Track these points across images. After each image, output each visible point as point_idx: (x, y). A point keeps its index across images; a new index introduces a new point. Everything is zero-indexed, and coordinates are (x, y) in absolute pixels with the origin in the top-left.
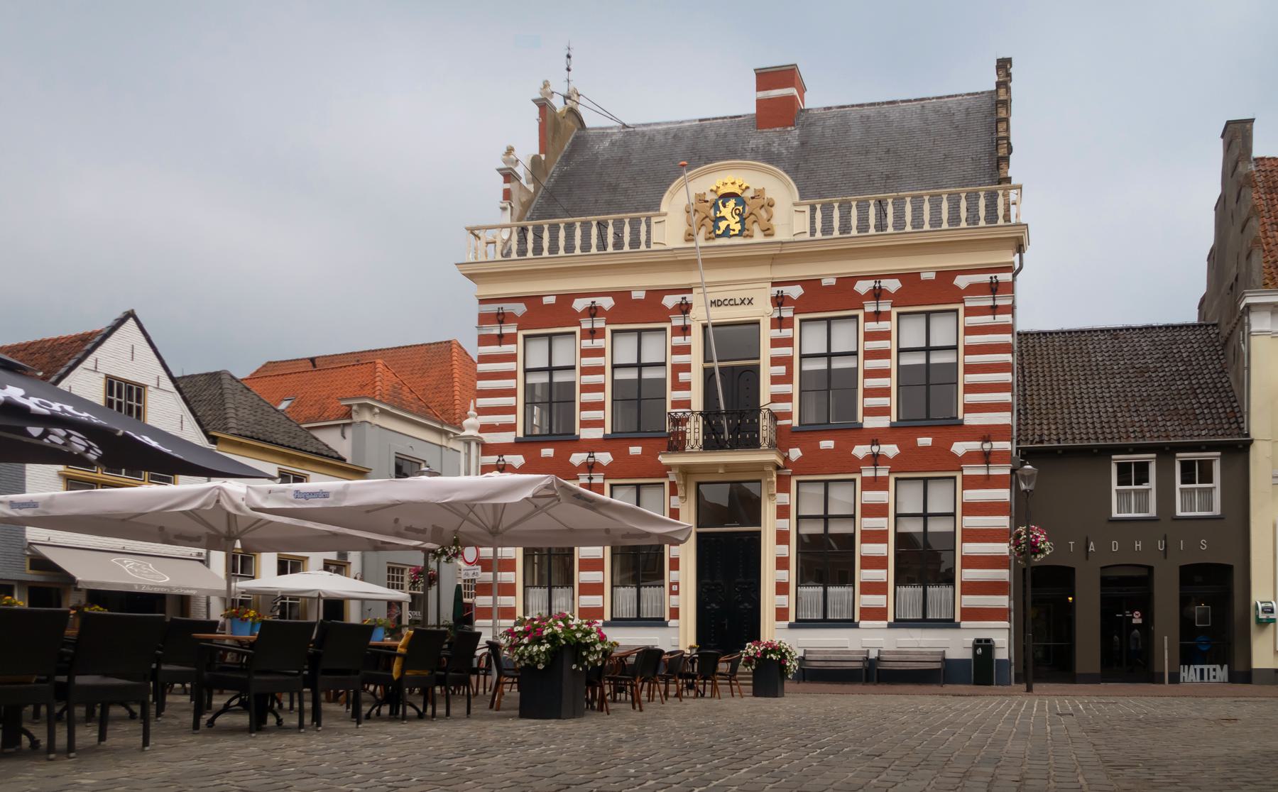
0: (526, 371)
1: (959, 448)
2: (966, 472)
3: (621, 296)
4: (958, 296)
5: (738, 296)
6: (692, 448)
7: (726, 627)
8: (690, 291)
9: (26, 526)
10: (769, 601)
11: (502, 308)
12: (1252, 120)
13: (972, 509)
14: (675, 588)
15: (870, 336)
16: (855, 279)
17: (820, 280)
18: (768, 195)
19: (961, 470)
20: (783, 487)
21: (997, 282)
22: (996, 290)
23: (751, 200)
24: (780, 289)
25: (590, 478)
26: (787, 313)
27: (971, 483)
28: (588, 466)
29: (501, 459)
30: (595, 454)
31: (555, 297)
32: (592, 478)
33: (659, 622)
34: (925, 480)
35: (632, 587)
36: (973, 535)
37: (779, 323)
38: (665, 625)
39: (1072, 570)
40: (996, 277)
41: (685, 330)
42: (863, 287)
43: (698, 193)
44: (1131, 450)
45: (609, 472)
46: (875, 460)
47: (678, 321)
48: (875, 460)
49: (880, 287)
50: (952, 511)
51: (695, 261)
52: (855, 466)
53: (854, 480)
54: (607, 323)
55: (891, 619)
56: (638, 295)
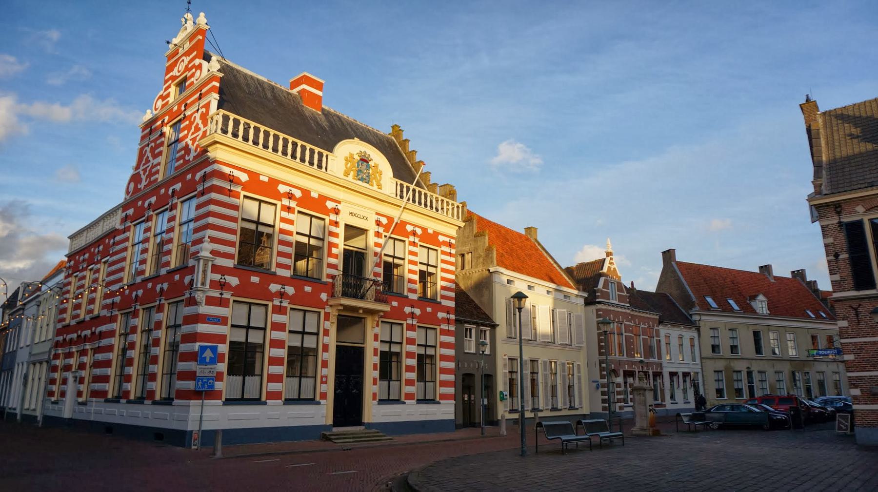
1: (441, 315)
3: (306, 192)
4: (440, 244)
5: (362, 214)
8: (339, 202)
12: (416, 152)
13: (444, 345)
16: (327, 198)
18: (380, 168)
19: (440, 326)
23: (373, 168)
24: (379, 217)
28: (221, 285)
29: (223, 277)
30: (285, 287)
32: (280, 302)
33: (311, 401)
35: (240, 376)
36: (444, 358)
43: (538, 231)
45: (236, 291)
46: (282, 295)
47: (333, 217)
48: (282, 295)
50: (263, 326)
52: (270, 296)
53: (266, 306)
54: (384, 231)
56: (430, 231)
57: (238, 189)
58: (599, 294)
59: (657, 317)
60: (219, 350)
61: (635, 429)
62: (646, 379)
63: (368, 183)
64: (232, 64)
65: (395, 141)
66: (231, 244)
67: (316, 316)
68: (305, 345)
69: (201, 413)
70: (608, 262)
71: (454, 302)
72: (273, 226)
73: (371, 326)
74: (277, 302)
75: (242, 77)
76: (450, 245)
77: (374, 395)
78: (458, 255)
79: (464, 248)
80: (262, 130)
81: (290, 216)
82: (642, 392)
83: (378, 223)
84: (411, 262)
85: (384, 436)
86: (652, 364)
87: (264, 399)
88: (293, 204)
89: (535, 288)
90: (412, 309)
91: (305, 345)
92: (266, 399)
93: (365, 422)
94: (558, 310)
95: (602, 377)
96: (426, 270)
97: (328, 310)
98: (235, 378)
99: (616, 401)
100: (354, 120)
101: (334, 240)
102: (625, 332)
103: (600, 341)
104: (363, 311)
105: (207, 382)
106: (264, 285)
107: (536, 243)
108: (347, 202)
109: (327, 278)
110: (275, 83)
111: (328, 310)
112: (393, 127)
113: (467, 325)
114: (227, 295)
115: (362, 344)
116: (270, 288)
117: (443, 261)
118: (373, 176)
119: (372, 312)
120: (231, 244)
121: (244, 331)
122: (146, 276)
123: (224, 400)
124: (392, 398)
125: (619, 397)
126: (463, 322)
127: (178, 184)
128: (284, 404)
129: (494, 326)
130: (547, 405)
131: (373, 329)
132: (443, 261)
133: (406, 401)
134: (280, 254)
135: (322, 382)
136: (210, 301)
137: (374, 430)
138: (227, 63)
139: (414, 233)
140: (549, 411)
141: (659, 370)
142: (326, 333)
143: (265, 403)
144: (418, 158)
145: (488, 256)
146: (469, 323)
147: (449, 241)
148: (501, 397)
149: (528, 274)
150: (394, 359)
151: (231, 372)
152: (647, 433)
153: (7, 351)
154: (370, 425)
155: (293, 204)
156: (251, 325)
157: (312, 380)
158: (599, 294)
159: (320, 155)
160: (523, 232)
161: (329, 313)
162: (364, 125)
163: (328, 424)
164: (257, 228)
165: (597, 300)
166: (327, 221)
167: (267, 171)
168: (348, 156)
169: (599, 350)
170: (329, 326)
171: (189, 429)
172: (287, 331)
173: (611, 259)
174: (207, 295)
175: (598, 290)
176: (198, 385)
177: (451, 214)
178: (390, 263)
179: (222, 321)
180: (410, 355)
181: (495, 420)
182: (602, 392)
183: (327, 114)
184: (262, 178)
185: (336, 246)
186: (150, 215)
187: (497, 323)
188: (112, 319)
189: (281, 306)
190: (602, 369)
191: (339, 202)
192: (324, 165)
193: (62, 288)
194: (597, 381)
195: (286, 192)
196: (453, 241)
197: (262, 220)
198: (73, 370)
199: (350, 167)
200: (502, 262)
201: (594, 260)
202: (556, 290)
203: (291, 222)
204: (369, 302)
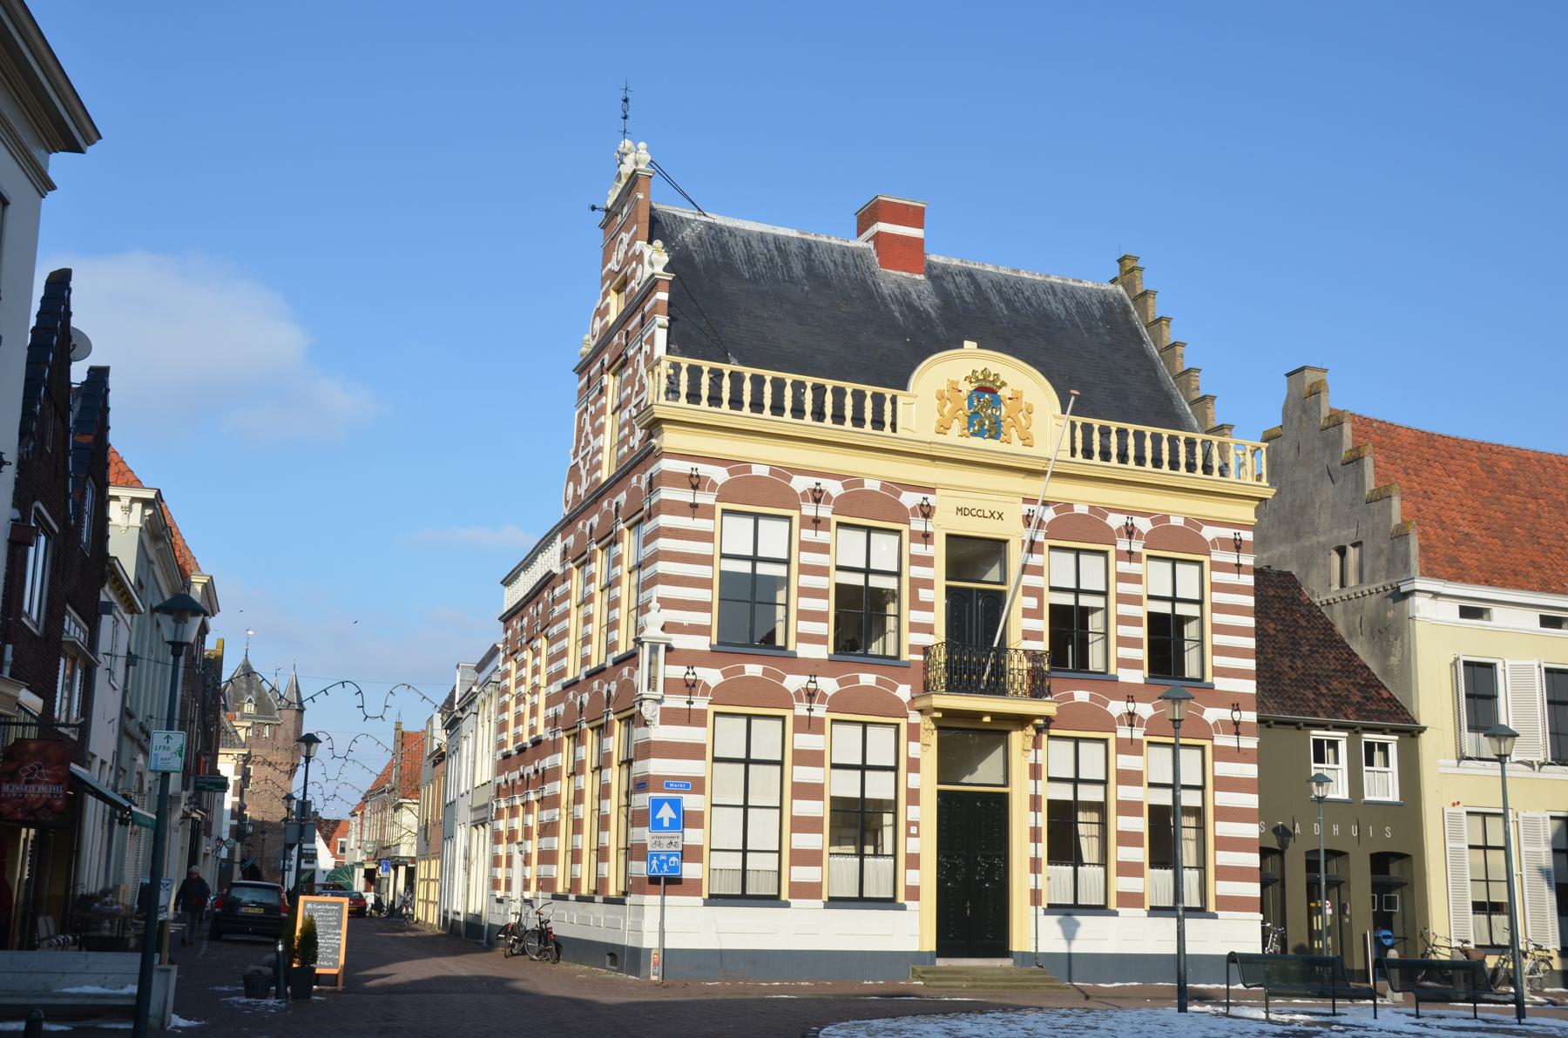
5: (988, 507)
8: (932, 490)
10: (1021, 881)
11: (696, 469)
13: (1224, 784)
15: (806, 546)
18: (1026, 399)
21: (1241, 540)
22: (1240, 547)
23: (1008, 401)
27: (1222, 754)
28: (687, 685)
32: (808, 710)
33: (889, 903)
40: (1239, 534)
41: (926, 537)
42: (1115, 521)
44: (1330, 727)
45: (835, 704)
47: (918, 525)
49: (1132, 525)
50: (779, 758)
51: (1044, 473)
52: (786, 700)
64: (720, 220)
66: (704, 607)
68: (867, 795)
74: (801, 709)
75: (741, 243)
76: (1238, 546)
77: (1036, 896)
88: (825, 511)
90: (1130, 704)
91: (867, 795)
105: (667, 862)
108: (947, 487)
109: (911, 652)
112: (1120, 261)
113: (1369, 737)
114: (700, 703)
117: (1217, 587)
118: (1009, 419)
119: (1022, 721)
120: (704, 607)
122: (592, 667)
126: (1301, 725)
127: (621, 494)
129: (1411, 732)
131: (1026, 754)
134: (804, 615)
136: (670, 717)
138: (711, 220)
142: (914, 766)
143: (787, 905)
144: (1170, 335)
146: (1324, 727)
147: (1233, 537)
153: (448, 802)
154: (1025, 957)
156: (752, 757)
159: (878, 400)
161: (918, 725)
164: (754, 568)
167: (763, 456)
170: (919, 751)
171: (645, 945)
176: (651, 866)
180: (1129, 808)
183: (937, 276)
186: (569, 569)
187: (1423, 724)
188: (556, 747)
191: (932, 490)
192: (888, 419)
193: (499, 683)
196: (1247, 536)
198: (520, 839)
199: (949, 412)
200: (1453, 561)
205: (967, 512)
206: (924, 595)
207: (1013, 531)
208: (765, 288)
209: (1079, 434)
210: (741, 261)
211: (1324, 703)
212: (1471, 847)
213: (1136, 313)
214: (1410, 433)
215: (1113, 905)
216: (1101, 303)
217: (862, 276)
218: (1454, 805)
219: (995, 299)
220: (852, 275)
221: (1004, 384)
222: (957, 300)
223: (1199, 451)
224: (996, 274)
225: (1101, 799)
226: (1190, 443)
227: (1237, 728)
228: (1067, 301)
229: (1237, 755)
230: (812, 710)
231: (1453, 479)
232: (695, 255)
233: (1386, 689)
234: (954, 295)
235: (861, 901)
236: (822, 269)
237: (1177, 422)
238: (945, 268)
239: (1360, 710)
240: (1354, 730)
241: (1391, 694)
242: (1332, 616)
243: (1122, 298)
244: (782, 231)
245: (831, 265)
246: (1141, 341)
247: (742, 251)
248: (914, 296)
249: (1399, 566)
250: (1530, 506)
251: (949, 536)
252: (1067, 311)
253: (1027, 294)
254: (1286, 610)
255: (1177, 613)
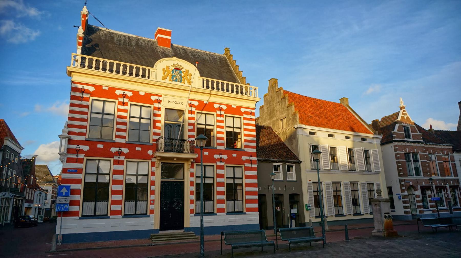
0: (92, 113)
1: (244, 158)
2: (246, 165)
3: (229, 106)
4: (242, 114)
5: (178, 101)
6: (186, 152)
7: (171, 216)
8: (161, 96)
9: (258, 179)
11: (84, 87)
13: (248, 177)
14: (152, 202)
16: (214, 103)
17: (231, 105)
20: (192, 166)
21: (251, 112)
23: (184, 72)
25: (119, 158)
26: (194, 109)
27: (247, 169)
29: (78, 146)
30: (122, 149)
31: (108, 87)
32: (120, 158)
33: (145, 215)
34: (234, 167)
35: (134, 201)
36: (248, 185)
37: (191, 112)
38: (149, 216)
39: (290, 195)
45: (227, 161)
46: (120, 154)
47: (156, 105)
48: (221, 160)
49: (221, 107)
52: (215, 161)
53: (214, 166)
55: (80, 216)
57: (88, 96)
58: (395, 135)
59: (451, 147)
60: (71, 188)
61: (374, 232)
62: (444, 191)
63: (181, 82)
64: (111, 30)
65: (226, 57)
67: (147, 164)
69: (61, 224)
70: (402, 113)
71: (256, 149)
72: (114, 115)
73: (187, 168)
77: (192, 211)
78: (280, 121)
79: (282, 116)
80: (235, 85)
81: (193, 116)
82: (377, 203)
83: (191, 105)
84: (218, 127)
85: (195, 236)
86: (449, 181)
87: (109, 215)
88: (222, 113)
89: (335, 136)
92: (110, 215)
93: (306, 222)
94: (356, 148)
95: (403, 191)
96: (232, 131)
97: (153, 160)
98: (230, 202)
99: (417, 207)
100: (197, 50)
101: (157, 118)
102: (421, 160)
103: (398, 167)
104: (177, 160)
106: (239, 158)
107: (347, 107)
109: (153, 141)
110: (141, 37)
111: (153, 160)
113: (288, 164)
115: (182, 179)
116: (111, 150)
117: (245, 124)
119: (187, 160)
121: (233, 180)
123: (195, 214)
124: (139, 213)
125: (419, 204)
128: (195, 216)
129: (298, 163)
130: (349, 211)
132: (245, 124)
133: (217, 213)
135: (151, 204)
137: (191, 232)
138: (110, 31)
139: (220, 109)
140: (369, 214)
141: (456, 184)
143: (109, 217)
144: (237, 64)
145: (294, 118)
146: (276, 161)
147: (249, 111)
148: (306, 208)
149: (329, 127)
150: (239, 187)
151: (228, 199)
152: (382, 234)
154: (189, 229)
155: (222, 113)
157: (241, 202)
158: (395, 135)
159: (144, 70)
160: (339, 102)
162: (204, 51)
163: (156, 229)
165: (394, 140)
166: (152, 108)
168: (165, 67)
169: (399, 173)
172: (225, 178)
173: (404, 111)
174: (67, 157)
175: (395, 132)
177: (253, 95)
178: (231, 132)
179: (79, 171)
181: (303, 222)
182: (403, 201)
184: (104, 88)
185: (159, 122)
189: (119, 160)
190: (402, 186)
191: (161, 96)
192: (147, 75)
194: (400, 194)
195: (156, 99)
197: (106, 112)
201: (393, 114)
202: (354, 135)
203: (222, 122)
204: (185, 154)
205: (172, 102)
206: (158, 125)
207: (185, 107)
208: (122, 47)
209: (205, 82)
210: (116, 40)
211: (276, 156)
212: (314, 191)
213: (228, 61)
214: (298, 95)
215: (215, 212)
216: (219, 58)
217: (152, 47)
218: (309, 181)
219: (190, 55)
220: (149, 46)
221: (183, 68)
222: (179, 54)
223: (239, 88)
224: (192, 50)
225: (241, 183)
226: (237, 86)
227: (251, 161)
228: (210, 57)
229: (251, 169)
230: (120, 158)
231: (308, 105)
232: (102, 37)
233: (292, 153)
234: (179, 53)
235: (135, 215)
236: (141, 44)
237: (234, 80)
238: (177, 47)
239: (286, 157)
240: (284, 162)
241: (294, 154)
242: (280, 136)
243: (225, 58)
244: (131, 35)
245: (144, 44)
246: (229, 66)
247: (117, 38)
248: (167, 52)
249: (295, 122)
250: (325, 111)
251: (166, 109)
252: (210, 59)
253: (199, 55)
254: (269, 135)
255: (234, 131)
